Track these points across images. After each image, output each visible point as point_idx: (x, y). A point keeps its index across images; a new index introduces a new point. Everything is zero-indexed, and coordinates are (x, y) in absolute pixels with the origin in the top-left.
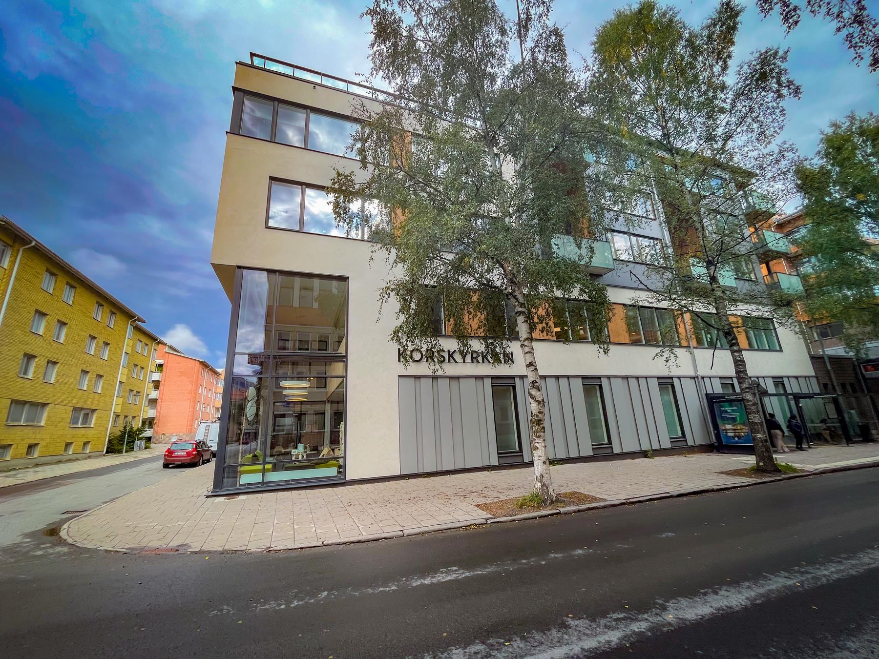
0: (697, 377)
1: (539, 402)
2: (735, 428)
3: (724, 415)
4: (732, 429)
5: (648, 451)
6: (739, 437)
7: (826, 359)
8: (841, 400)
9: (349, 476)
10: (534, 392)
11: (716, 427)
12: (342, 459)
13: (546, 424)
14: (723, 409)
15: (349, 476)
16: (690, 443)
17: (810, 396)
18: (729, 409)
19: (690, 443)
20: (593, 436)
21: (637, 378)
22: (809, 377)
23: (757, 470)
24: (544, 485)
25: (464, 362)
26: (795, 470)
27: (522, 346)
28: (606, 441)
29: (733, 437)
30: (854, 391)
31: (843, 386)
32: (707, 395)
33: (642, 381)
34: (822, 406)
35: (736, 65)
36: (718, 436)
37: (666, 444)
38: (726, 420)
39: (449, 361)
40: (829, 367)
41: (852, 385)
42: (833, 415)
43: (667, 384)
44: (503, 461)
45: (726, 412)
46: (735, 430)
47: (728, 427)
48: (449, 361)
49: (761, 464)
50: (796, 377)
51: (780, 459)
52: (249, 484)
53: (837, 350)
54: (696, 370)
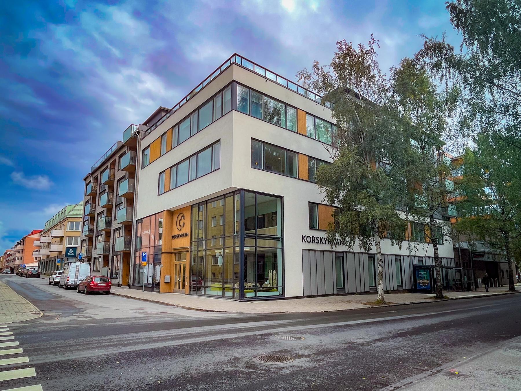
0: (410, 256)
1: (382, 267)
2: (424, 281)
3: (419, 275)
4: (422, 282)
5: (389, 291)
6: (425, 286)
7: (460, 250)
8: (462, 271)
9: (287, 295)
10: (381, 263)
11: (415, 280)
12: (276, 288)
13: (384, 275)
14: (420, 272)
15: (287, 295)
16: (404, 288)
17: (451, 268)
18: (422, 273)
19: (404, 288)
20: (398, 282)
21: (388, 255)
22: (452, 258)
23: (436, 297)
24: (382, 297)
25: (326, 243)
26: (448, 298)
27: (376, 245)
28: (342, 287)
29: (422, 286)
30: (467, 267)
31: (464, 263)
32: (413, 265)
33: (389, 256)
34: (454, 274)
35: (449, 44)
36: (415, 285)
37: (368, 290)
38: (421, 278)
39: (320, 243)
40: (460, 255)
41: (467, 263)
42: (458, 278)
43: (398, 258)
44: (338, 292)
45: (421, 274)
46: (424, 282)
47: (421, 281)
48: (320, 243)
49: (438, 295)
50: (447, 258)
51: (444, 294)
52: (263, 296)
53: (465, 245)
54: (253, 205)
